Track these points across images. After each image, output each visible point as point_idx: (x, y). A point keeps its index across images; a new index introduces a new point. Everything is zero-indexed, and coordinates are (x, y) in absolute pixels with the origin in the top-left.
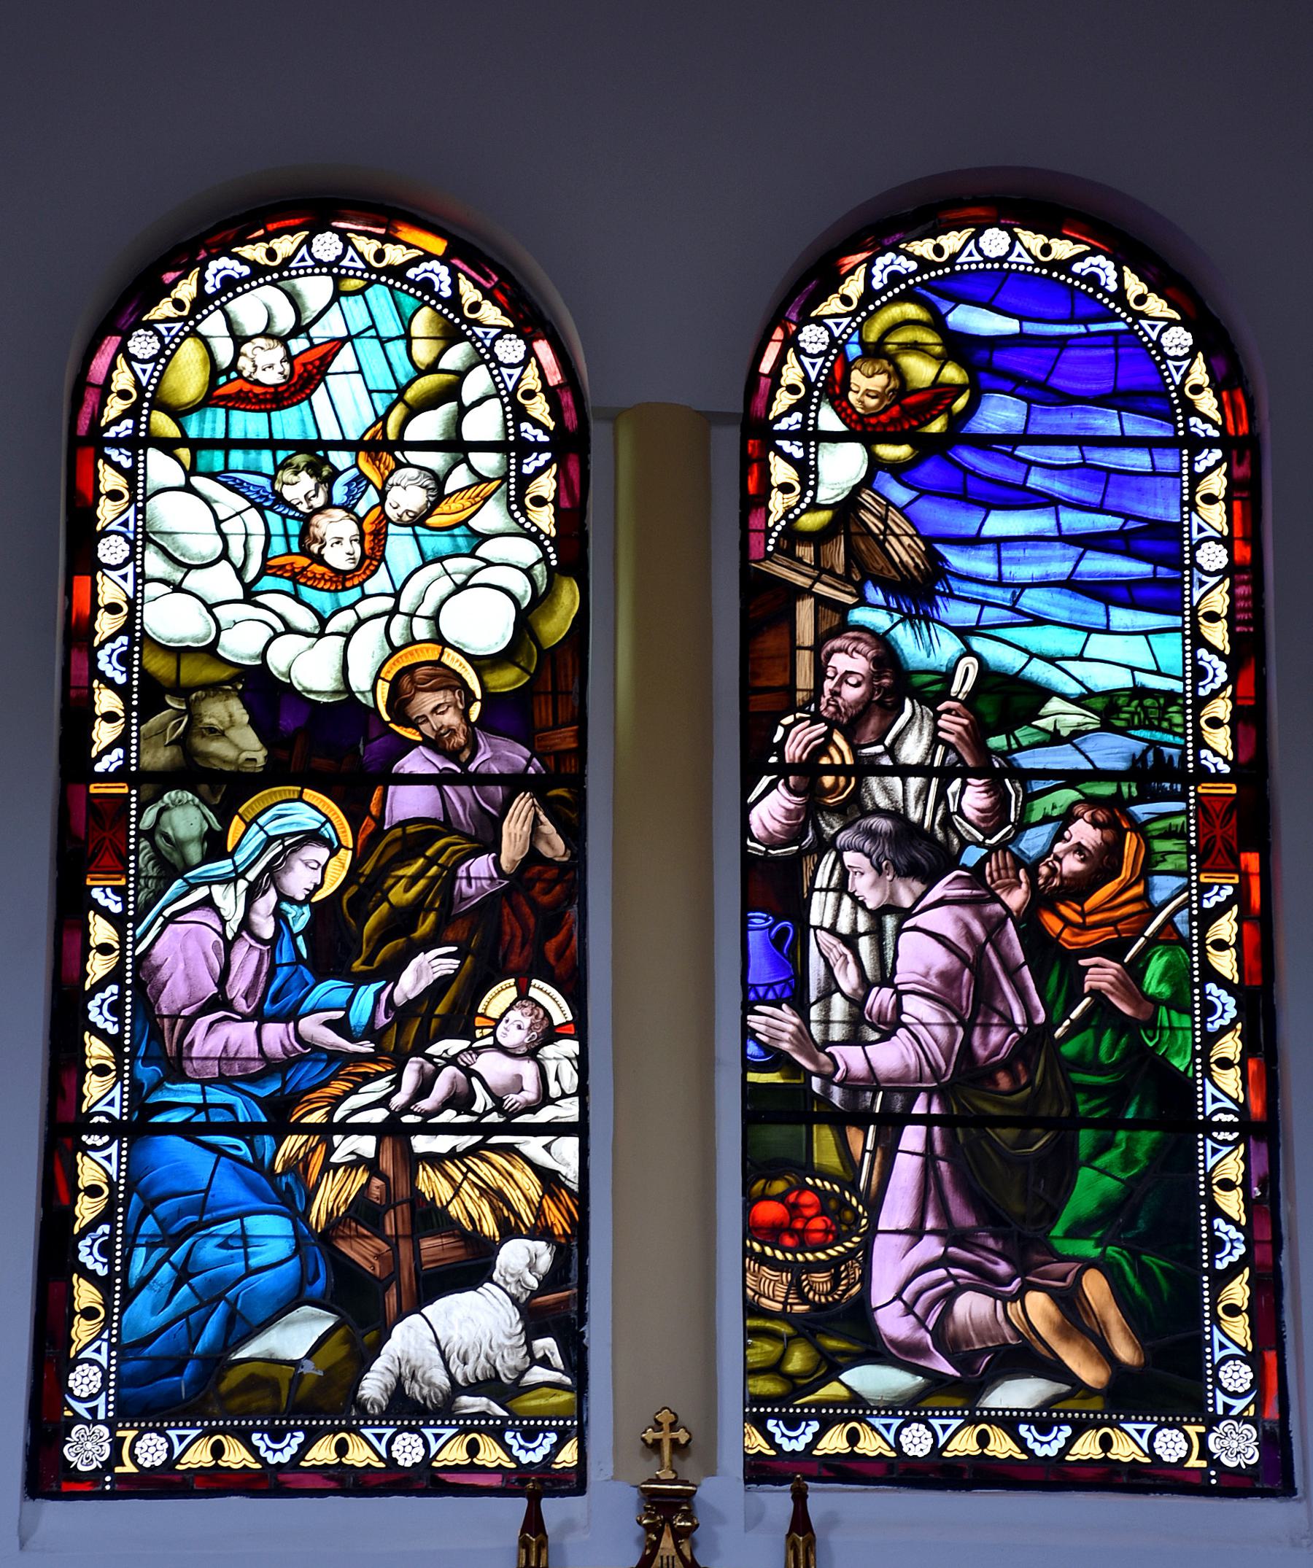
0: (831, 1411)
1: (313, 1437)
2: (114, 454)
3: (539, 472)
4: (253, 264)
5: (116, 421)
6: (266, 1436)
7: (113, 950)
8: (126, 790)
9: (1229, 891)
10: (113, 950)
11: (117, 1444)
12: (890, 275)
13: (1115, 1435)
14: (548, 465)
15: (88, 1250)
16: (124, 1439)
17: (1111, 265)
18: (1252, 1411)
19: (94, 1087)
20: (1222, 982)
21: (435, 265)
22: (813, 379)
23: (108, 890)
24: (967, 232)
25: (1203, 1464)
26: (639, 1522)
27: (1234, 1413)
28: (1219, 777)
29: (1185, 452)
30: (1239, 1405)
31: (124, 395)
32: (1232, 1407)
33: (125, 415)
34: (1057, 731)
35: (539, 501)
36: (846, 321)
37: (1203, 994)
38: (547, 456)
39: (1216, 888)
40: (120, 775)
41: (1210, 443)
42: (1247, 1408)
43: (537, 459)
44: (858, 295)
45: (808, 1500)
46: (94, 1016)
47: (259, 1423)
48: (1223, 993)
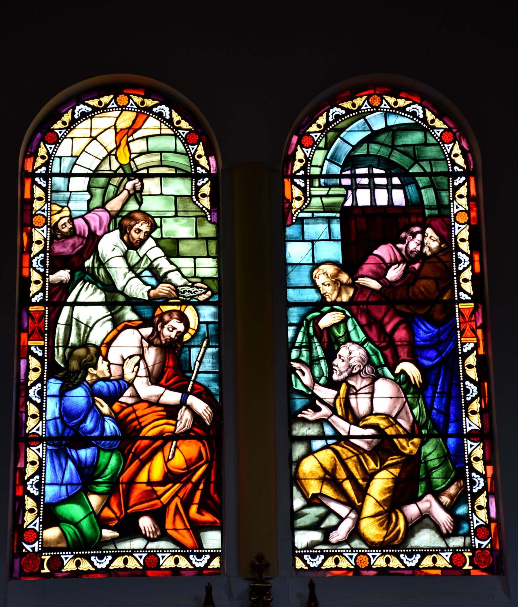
4: (93, 107)
5: (40, 167)
8: (43, 309)
9: (472, 345)
12: (335, 116)
15: (31, 486)
16: (44, 559)
18: (489, 546)
20: (472, 381)
22: (308, 156)
23: (37, 347)
24: (112, 96)
26: (250, 599)
28: (466, 301)
29: (451, 179)
31: (43, 157)
32: (482, 545)
35: (204, 196)
36: (319, 134)
37: (464, 385)
38: (463, 178)
40: (42, 303)
42: (487, 545)
43: (203, 180)
44: (336, 360)
45: (315, 590)
48: (472, 385)
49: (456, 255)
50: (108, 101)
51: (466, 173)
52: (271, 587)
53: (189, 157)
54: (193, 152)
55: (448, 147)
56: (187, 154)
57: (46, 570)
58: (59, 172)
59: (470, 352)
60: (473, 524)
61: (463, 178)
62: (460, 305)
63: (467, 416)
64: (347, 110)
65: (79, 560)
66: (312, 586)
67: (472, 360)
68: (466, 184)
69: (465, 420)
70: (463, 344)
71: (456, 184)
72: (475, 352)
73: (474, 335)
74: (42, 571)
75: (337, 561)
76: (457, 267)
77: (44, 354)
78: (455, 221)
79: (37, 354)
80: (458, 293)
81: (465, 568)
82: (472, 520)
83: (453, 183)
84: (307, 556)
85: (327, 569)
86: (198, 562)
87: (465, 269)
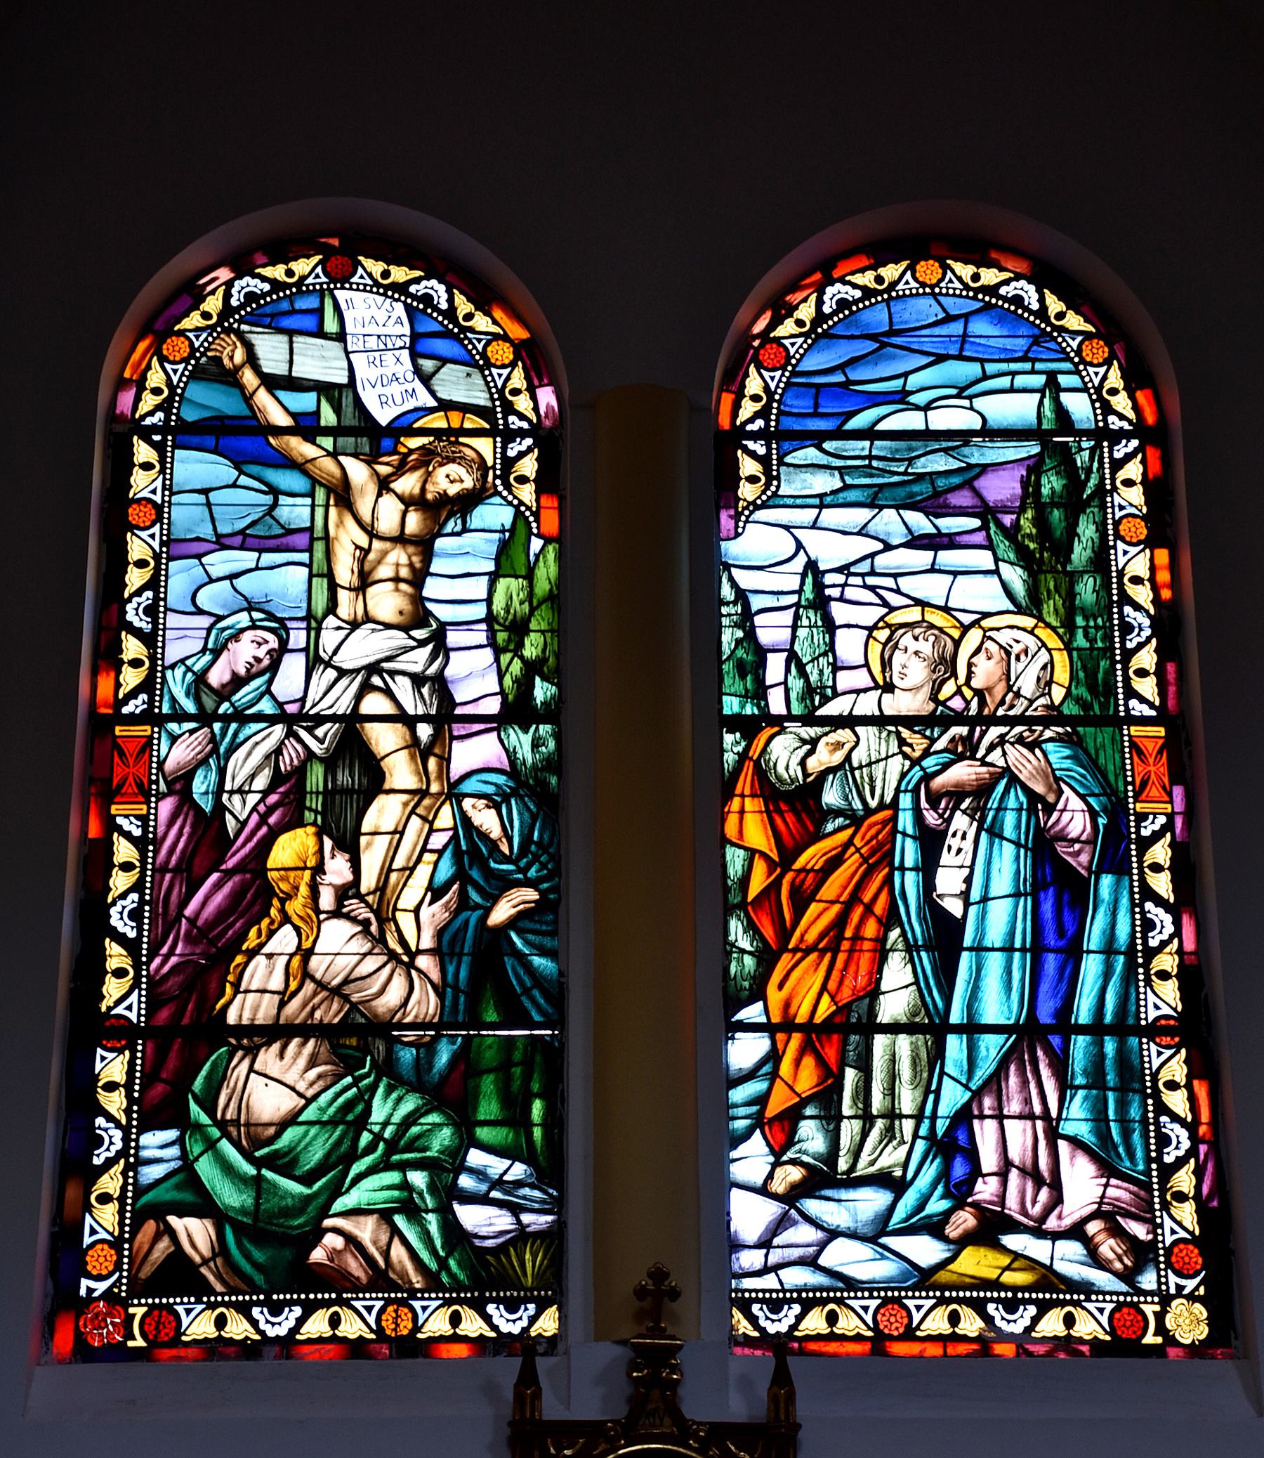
0: (502, 1294)
1: (309, 1309)
2: (751, 445)
3: (521, 455)
4: (864, 289)
6: (265, 1310)
7: (134, 867)
9: (1162, 820)
10: (134, 867)
11: (1152, 1293)
13: (1079, 1314)
14: (529, 450)
16: (134, 1315)
17: (247, 279)
18: (1202, 1291)
19: (113, 988)
21: (238, 284)
24: (904, 264)
25: (1159, 1340)
27: (1186, 1292)
28: (1143, 721)
30: (1190, 1284)
31: (755, 398)
32: (1184, 1287)
33: (158, 408)
34: (235, 675)
35: (522, 480)
38: (1135, 443)
39: (1151, 817)
41: (522, 434)
42: (1197, 1288)
46: (115, 921)
47: (494, 1294)
49: (1121, 613)
50: (896, 275)
51: (1139, 430)
52: (680, 1347)
53: (1090, 395)
54: (1096, 381)
55: (1096, 374)
56: (1085, 389)
57: (139, 1342)
58: (923, 427)
59: (1156, 836)
60: (1163, 1234)
61: (1135, 443)
62: (1132, 728)
63: (1148, 982)
64: (452, 308)
65: (336, 1313)
66: (782, 1378)
67: (1160, 853)
68: (1140, 456)
69: (1145, 993)
70: (1141, 817)
71: (1118, 455)
72: (1168, 835)
73: (1166, 798)
74: (130, 1344)
75: (832, 1319)
76: (1123, 642)
77: (140, 935)
78: (1118, 536)
79: (1153, 831)
80: (1126, 700)
81: (1145, 1341)
82: (1161, 1226)
83: (1111, 452)
84: (994, 1305)
85: (808, 1338)
86: (773, 1321)
87: (1141, 646)
